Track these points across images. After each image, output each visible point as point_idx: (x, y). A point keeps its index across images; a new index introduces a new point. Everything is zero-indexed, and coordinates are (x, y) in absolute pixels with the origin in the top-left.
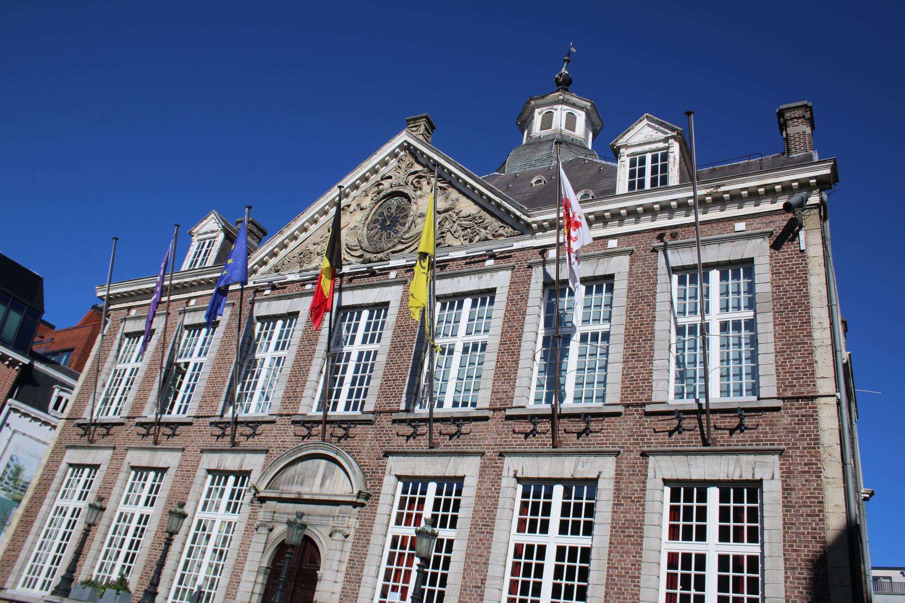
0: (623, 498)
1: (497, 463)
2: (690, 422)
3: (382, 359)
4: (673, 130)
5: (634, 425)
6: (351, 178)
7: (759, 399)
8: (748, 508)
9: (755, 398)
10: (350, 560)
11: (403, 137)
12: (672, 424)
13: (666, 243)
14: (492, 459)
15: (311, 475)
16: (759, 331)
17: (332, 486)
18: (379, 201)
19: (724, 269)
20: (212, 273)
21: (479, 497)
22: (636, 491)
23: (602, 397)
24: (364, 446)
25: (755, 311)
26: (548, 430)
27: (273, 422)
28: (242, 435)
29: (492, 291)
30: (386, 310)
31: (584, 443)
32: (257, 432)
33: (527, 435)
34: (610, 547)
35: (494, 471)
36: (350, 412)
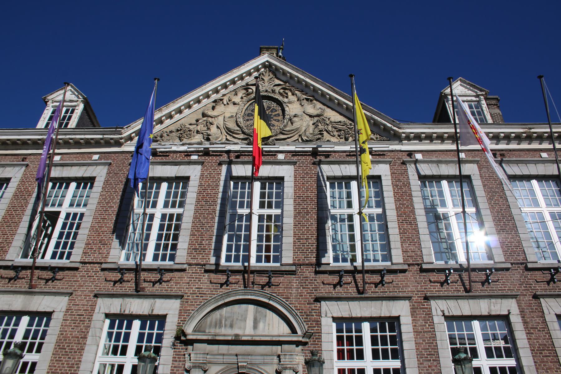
0: (531, 328)
1: (424, 305)
2: (348, 279)
3: (288, 221)
4: (481, 91)
5: (520, 277)
6: (223, 79)
7: (392, 264)
8: (356, 336)
11: (264, 58)
12: (547, 277)
14: (419, 302)
15: (240, 318)
16: (284, 222)
17: (267, 328)
19: (263, 181)
20: (85, 134)
21: (416, 332)
22: (539, 323)
24: (291, 293)
26: (458, 280)
28: (145, 281)
29: (92, 180)
30: (8, 184)
31: (486, 290)
32: (164, 279)
33: (442, 284)
34: (536, 365)
35: (423, 311)
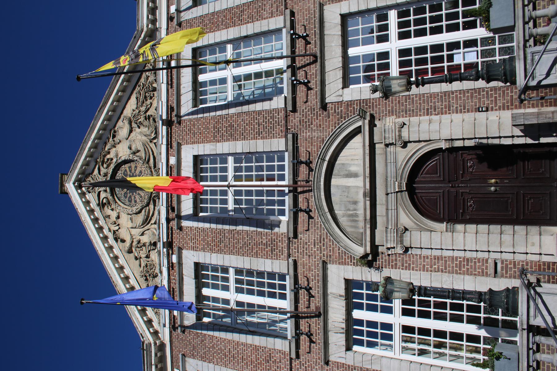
2: (301, 75)
9: (284, 31)
10: (428, 115)
13: (179, 326)
15: (346, 194)
18: (115, 200)
23: (282, 277)
25: (230, 267)
27: (295, 263)
33: (309, 89)
36: (288, 292)
